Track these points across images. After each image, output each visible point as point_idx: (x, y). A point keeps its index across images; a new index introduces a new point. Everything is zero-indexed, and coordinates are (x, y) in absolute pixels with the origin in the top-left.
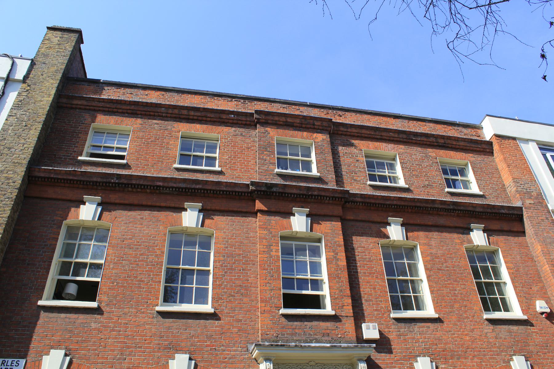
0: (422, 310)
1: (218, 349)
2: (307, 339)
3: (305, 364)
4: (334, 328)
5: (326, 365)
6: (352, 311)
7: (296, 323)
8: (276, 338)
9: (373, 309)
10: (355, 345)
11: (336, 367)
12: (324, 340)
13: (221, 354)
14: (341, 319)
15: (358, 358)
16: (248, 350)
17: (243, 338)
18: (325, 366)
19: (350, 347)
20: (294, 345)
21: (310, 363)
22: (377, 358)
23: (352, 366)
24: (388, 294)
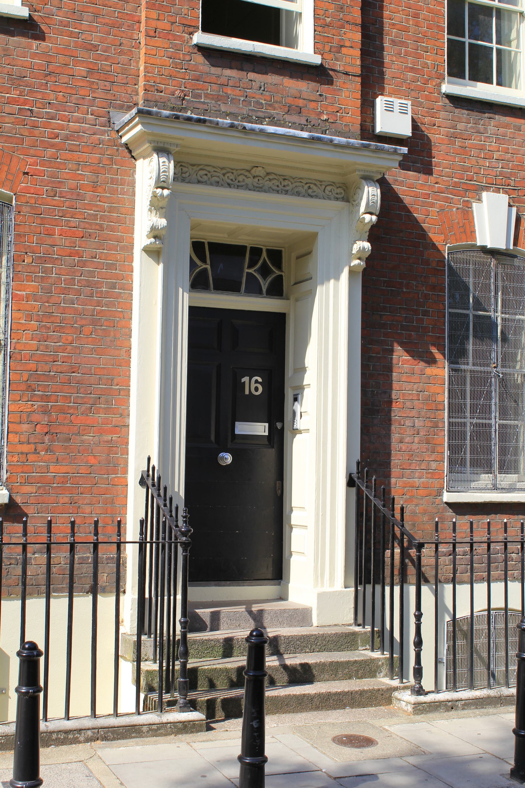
0: (505, 86)
1: (38, 113)
2: (250, 114)
3: (242, 172)
4: (315, 96)
5: (289, 180)
6: (358, 62)
7: (228, 72)
8: (179, 103)
9: (406, 67)
10: (363, 144)
11: (309, 188)
12: (289, 122)
13: (46, 125)
14: (332, 77)
15: (362, 173)
16: (109, 121)
17: (100, 93)
18: (286, 181)
19: (352, 145)
20: (227, 124)
21: (253, 171)
22: (396, 180)
23: (344, 191)
24: (444, 35)
